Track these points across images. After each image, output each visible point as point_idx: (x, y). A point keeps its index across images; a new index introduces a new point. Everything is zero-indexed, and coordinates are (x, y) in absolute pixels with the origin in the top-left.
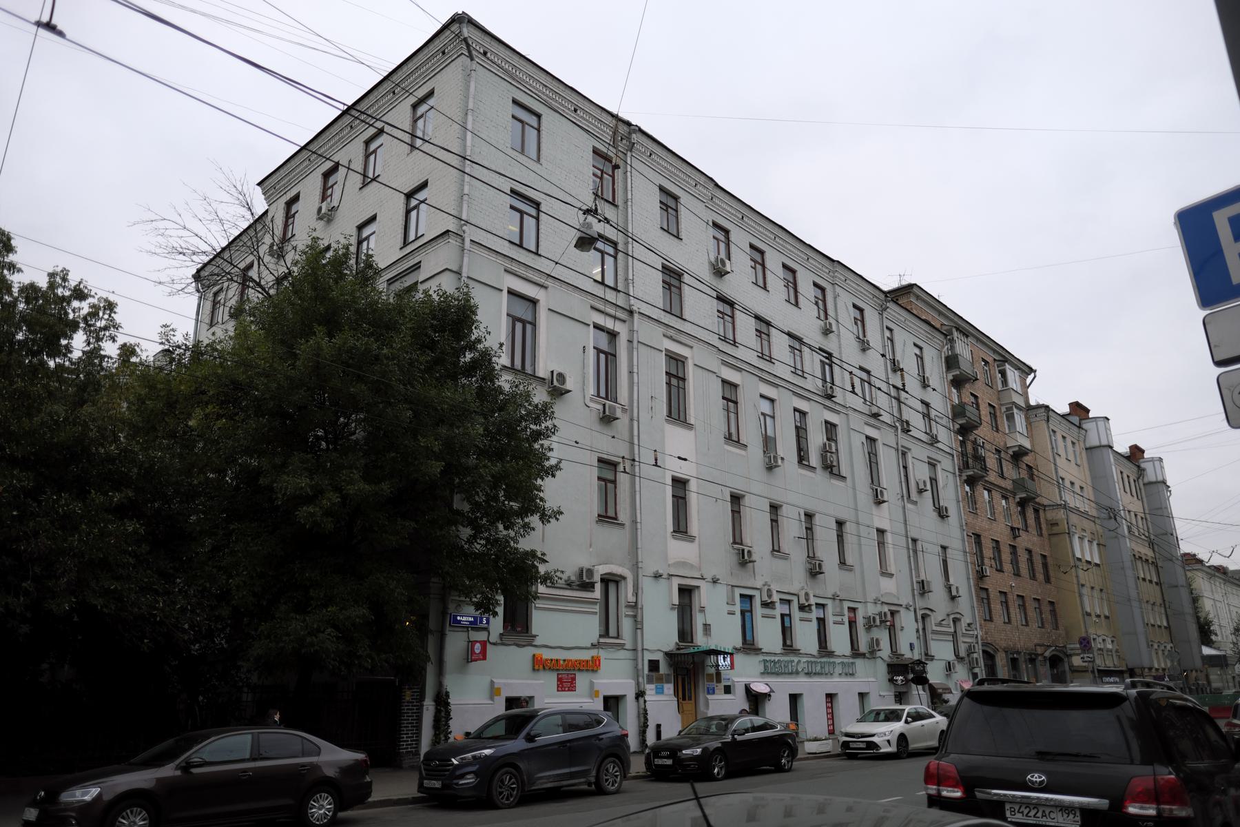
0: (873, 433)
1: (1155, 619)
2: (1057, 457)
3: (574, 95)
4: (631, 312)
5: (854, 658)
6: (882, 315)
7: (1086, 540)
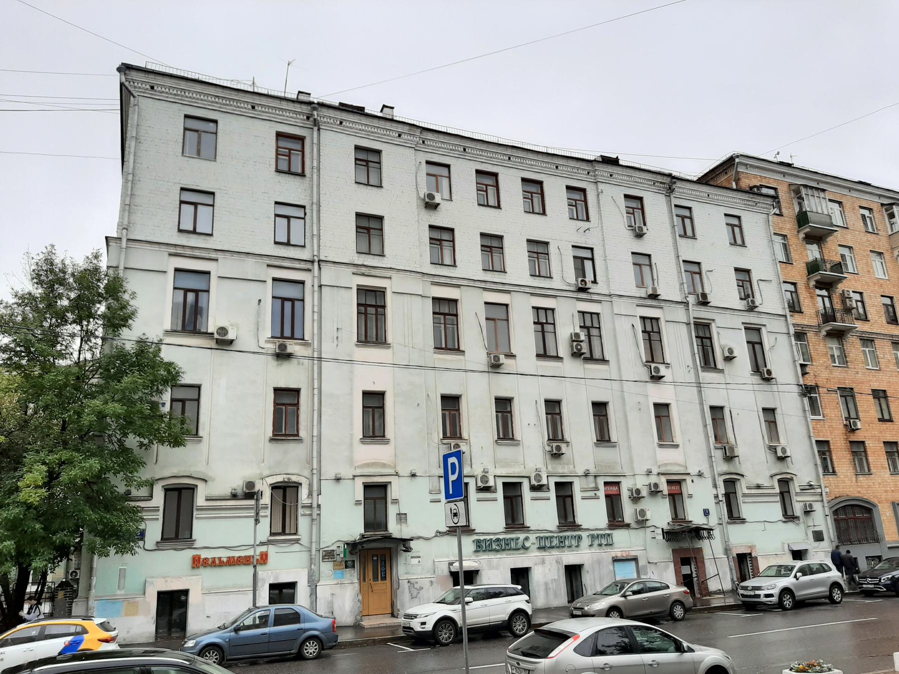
5: (610, 529)
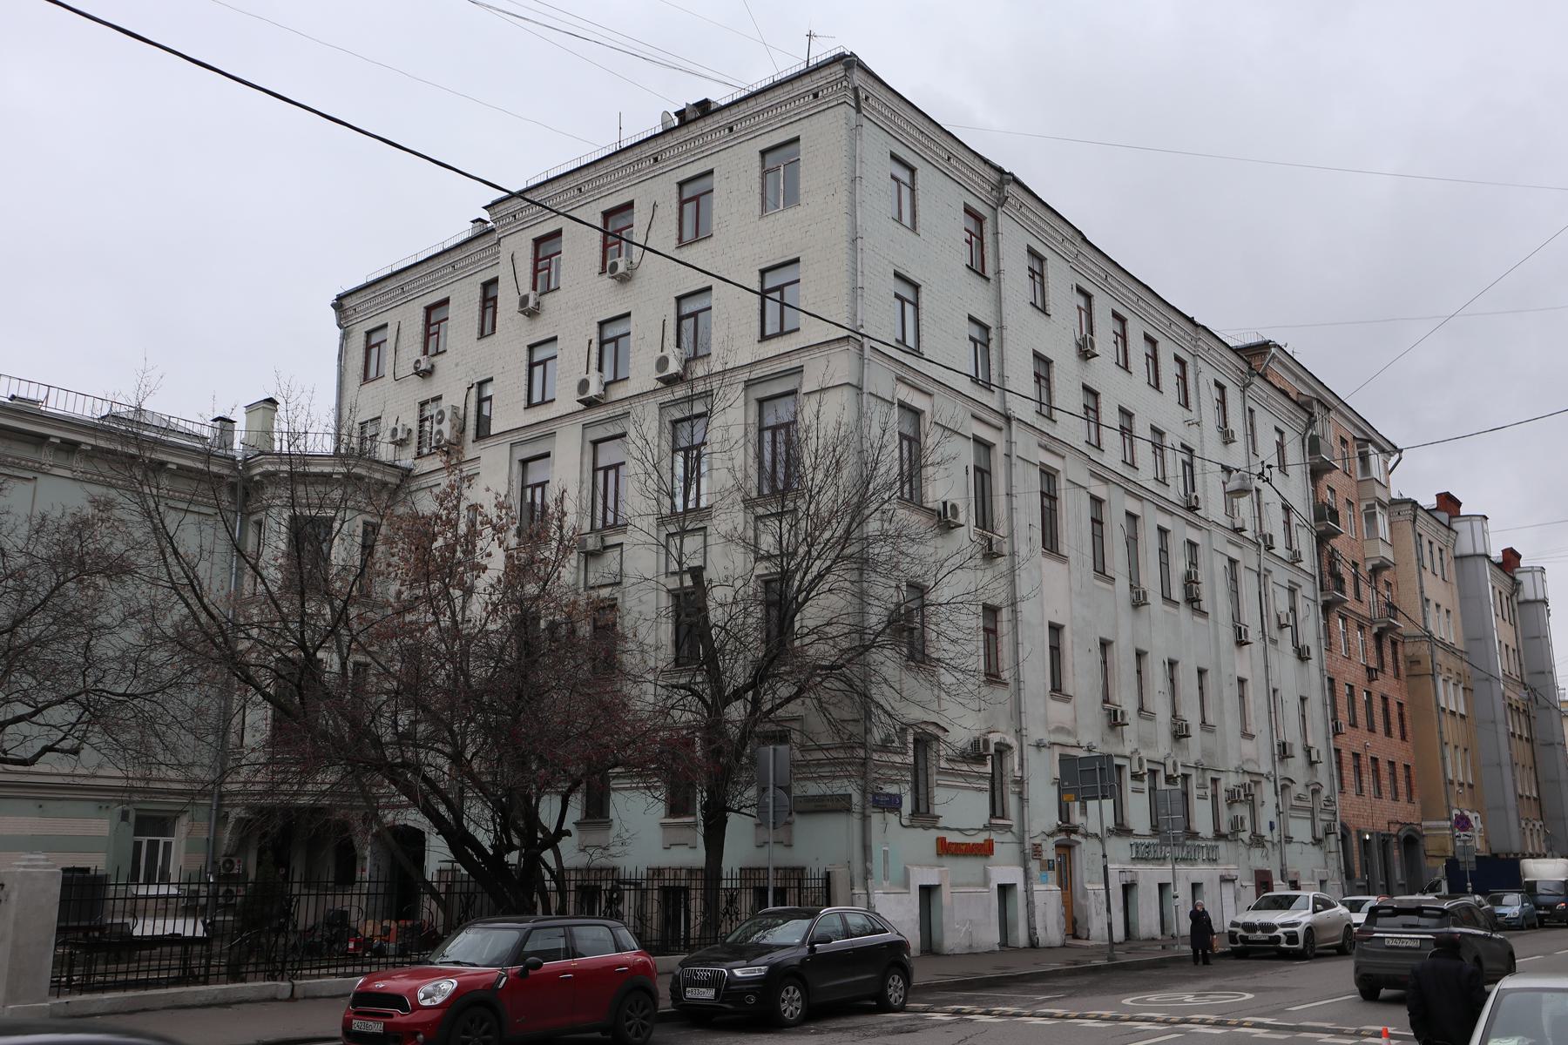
0: (1234, 553)
1: (1523, 790)
2: (1423, 570)
3: (949, 140)
4: (1008, 419)
6: (1243, 392)
7: (1451, 683)
